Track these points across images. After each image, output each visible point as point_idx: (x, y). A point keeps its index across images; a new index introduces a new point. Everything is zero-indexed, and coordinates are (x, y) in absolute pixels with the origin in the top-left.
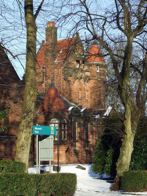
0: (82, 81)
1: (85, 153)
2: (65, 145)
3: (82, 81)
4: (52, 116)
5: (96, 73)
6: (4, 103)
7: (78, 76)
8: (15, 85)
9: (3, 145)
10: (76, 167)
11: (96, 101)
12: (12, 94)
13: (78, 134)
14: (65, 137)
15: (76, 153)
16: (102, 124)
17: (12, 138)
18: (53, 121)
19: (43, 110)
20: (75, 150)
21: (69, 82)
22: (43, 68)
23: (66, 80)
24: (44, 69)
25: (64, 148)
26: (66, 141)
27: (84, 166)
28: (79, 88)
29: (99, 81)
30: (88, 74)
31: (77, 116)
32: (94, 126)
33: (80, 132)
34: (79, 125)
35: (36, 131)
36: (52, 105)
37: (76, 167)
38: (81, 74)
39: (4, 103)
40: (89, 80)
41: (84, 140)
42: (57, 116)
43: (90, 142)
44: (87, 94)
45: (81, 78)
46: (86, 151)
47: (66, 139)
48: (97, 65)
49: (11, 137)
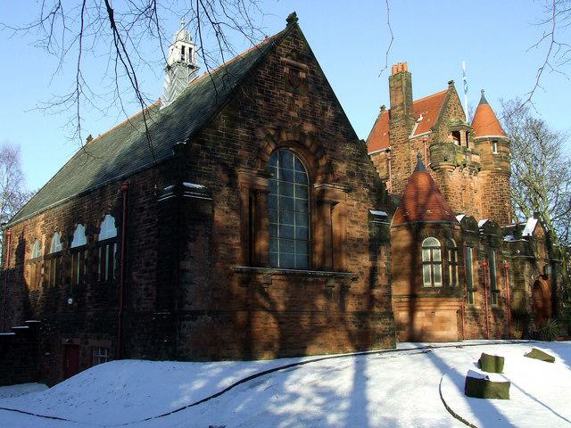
0: (466, 171)
1: (491, 315)
2: (458, 296)
3: (466, 171)
4: (425, 231)
5: (491, 156)
6: (323, 191)
7: (459, 162)
8: (349, 149)
9: (322, 296)
10: (527, 355)
11: (496, 211)
12: (340, 169)
13: (477, 273)
14: (454, 280)
15: (475, 314)
16: (521, 254)
17: (343, 278)
18: (426, 243)
19: (406, 219)
20: (473, 309)
21: (442, 172)
22: (387, 151)
23: (435, 170)
24: (389, 154)
25: (457, 304)
26: (460, 288)
27: (548, 351)
28: (462, 186)
29: (498, 172)
30: (476, 158)
31: (472, 234)
32: (506, 258)
33: (479, 271)
34: (477, 258)
35: (439, 244)
36: (424, 207)
37: (527, 355)
38: (464, 157)
39: (323, 191)
40: (479, 170)
41: (488, 288)
42: (438, 230)
43: (498, 291)
44: (478, 197)
45: (465, 165)
46: (494, 310)
47: (457, 284)
48: (494, 142)
49: (342, 274)
